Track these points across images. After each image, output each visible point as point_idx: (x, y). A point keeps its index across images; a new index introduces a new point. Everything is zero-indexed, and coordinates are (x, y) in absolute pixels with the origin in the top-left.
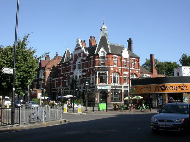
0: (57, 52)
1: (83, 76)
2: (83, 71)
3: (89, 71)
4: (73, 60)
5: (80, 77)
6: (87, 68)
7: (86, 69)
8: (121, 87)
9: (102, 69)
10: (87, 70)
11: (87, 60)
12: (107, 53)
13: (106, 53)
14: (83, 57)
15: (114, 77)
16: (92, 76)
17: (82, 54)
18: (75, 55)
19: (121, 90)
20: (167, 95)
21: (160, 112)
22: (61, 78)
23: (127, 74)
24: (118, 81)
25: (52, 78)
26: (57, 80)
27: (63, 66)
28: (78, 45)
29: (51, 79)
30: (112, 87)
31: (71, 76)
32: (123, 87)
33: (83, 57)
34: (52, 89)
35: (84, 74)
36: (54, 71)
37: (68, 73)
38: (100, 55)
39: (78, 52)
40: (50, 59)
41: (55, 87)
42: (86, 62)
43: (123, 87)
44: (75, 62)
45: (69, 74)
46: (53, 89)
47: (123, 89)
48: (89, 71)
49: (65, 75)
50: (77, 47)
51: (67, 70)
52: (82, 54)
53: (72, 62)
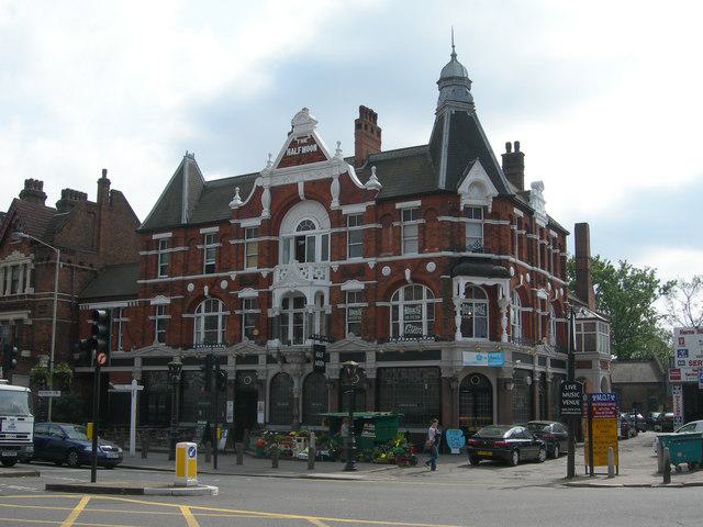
0: (105, 172)
4: (266, 213)
5: (320, 297)
6: (377, 255)
10: (379, 266)
11: (376, 220)
12: (496, 193)
13: (493, 191)
15: (207, 318)
17: (335, 187)
20: (489, 418)
26: (126, 311)
27: (173, 242)
31: (249, 293)
32: (138, 362)
37: (218, 280)
38: (464, 202)
39: (300, 176)
42: (373, 226)
43: (138, 362)
44: (272, 226)
45: (224, 284)
48: (191, 287)
52: (335, 187)
53: (246, 223)
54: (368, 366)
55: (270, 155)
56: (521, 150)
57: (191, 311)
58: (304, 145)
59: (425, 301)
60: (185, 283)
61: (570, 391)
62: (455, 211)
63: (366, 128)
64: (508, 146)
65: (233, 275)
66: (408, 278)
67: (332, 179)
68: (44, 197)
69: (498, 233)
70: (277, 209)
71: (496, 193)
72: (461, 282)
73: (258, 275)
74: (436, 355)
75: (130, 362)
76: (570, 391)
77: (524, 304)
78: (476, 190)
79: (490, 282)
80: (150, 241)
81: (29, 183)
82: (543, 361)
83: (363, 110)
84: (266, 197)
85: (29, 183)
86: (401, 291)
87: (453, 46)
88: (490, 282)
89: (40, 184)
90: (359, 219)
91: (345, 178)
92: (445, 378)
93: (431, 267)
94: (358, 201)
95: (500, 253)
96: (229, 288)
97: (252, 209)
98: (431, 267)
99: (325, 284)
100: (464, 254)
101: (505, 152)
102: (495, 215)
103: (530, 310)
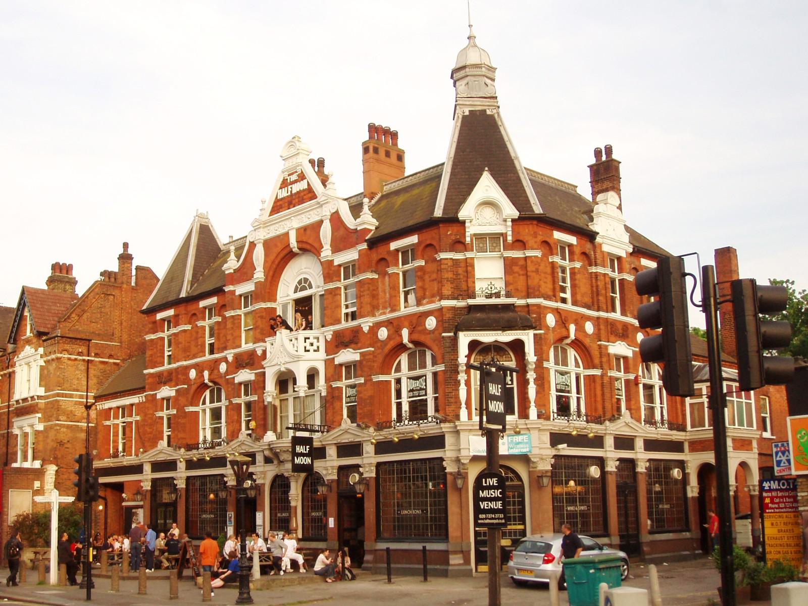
0: (126, 246)
1: (334, 371)
2: (340, 342)
3: (383, 333)
4: (259, 274)
5: (312, 377)
8: (598, 442)
9: (493, 315)
12: (515, 214)
13: (511, 212)
14: (336, 249)
16: (212, 402)
18: (267, 244)
19: (681, 464)
20: (522, 527)
22: (166, 392)
23: (625, 358)
24: (578, 399)
25: (98, 398)
26: (126, 410)
28: (294, 177)
29: (88, 407)
30: (556, 439)
31: (245, 375)
32: (609, 442)
33: (336, 249)
35: (348, 356)
36: (111, 356)
37: (217, 362)
38: (471, 230)
40: (80, 290)
41: (116, 455)
43: (609, 442)
44: (268, 290)
45: (223, 367)
46: (108, 462)
47: (612, 455)
48: (193, 374)
49: (193, 374)
50: (284, 194)
51: (208, 341)
53: (242, 289)
54: (366, 461)
55: (263, 202)
56: (614, 156)
57: (194, 402)
58: (295, 182)
59: (429, 370)
60: (187, 368)
61: (490, 488)
62: (459, 244)
63: (388, 154)
64: (598, 153)
65: (230, 354)
66: (405, 340)
67: (321, 222)
68: (73, 282)
69: (525, 267)
70: (273, 262)
71: (515, 214)
72: (465, 339)
73: (252, 353)
74: (438, 442)
75: (598, 442)
76: (490, 488)
77: (589, 363)
78: (488, 212)
79: (506, 337)
80: (155, 322)
81: (56, 267)
82: (623, 442)
83: (374, 129)
84: (259, 255)
85: (56, 267)
86: (404, 359)
87: (470, 26)
88: (506, 337)
89: (68, 268)
90: (350, 269)
91: (336, 218)
92: (451, 474)
93: (431, 323)
94: (352, 245)
95: (528, 296)
96: (227, 373)
97: (245, 272)
98: (431, 323)
99: (318, 360)
100: (471, 302)
101: (593, 161)
102: (520, 244)
103: (597, 372)
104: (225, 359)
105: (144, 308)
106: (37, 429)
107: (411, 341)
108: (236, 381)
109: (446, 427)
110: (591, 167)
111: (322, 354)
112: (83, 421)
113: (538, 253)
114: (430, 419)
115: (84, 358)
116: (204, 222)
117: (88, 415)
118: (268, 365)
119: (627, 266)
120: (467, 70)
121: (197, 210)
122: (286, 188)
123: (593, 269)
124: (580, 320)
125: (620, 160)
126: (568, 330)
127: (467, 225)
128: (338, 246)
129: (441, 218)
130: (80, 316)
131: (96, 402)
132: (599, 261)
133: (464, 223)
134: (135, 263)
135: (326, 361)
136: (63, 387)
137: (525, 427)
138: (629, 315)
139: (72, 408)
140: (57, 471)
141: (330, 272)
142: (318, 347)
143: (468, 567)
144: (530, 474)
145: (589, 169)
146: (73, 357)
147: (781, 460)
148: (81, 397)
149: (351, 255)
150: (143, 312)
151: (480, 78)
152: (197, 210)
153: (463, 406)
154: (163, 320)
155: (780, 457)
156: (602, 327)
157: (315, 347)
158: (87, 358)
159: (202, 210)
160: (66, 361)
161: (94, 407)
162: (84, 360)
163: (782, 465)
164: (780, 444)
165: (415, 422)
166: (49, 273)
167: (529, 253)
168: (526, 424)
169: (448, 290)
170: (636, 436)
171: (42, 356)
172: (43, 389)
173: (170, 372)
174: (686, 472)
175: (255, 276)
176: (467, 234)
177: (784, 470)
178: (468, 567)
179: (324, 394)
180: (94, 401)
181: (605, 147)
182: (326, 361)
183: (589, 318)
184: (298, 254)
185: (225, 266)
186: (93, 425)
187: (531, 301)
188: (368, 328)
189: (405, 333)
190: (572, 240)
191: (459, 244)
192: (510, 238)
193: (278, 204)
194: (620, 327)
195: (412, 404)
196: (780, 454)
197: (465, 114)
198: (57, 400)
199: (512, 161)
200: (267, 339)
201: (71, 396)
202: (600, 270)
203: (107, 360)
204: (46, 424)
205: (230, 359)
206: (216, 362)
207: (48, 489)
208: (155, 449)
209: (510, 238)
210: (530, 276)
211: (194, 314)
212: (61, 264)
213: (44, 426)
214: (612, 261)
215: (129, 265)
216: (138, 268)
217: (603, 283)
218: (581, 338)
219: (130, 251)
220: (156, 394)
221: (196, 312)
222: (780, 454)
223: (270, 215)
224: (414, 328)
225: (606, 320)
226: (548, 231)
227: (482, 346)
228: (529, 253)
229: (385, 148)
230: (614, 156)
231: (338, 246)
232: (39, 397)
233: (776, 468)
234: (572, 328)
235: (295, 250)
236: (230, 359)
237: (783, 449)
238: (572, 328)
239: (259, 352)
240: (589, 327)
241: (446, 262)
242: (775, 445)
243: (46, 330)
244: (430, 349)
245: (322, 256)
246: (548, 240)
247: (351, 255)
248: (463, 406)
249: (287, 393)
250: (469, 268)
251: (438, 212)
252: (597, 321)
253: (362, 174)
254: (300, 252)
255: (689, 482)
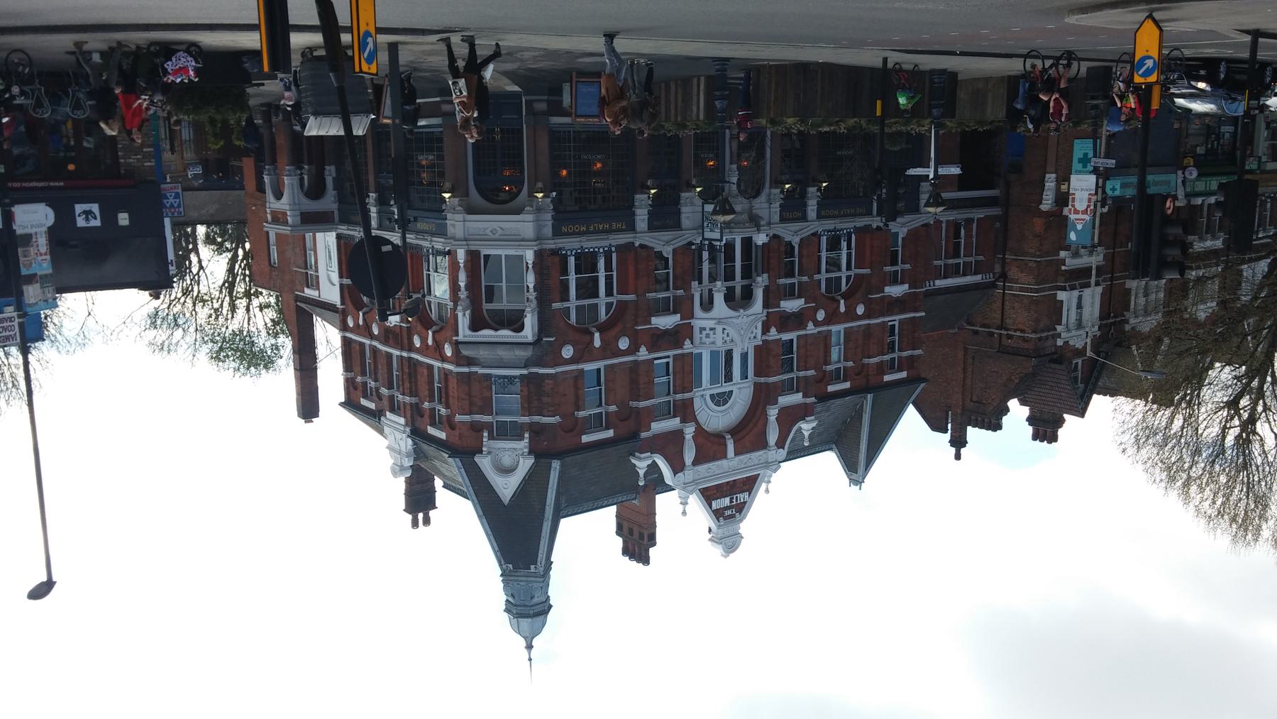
0: (958, 457)
1: (682, 307)
4: (773, 413)
7: (780, 331)
10: (633, 349)
12: (477, 459)
13: (484, 462)
14: (678, 436)
18: (763, 445)
21: (464, 134)
25: (993, 285)
31: (792, 305)
33: (678, 436)
34: (995, 211)
36: (976, 332)
38: (523, 445)
39: (730, 466)
42: (643, 404)
44: (763, 396)
45: (821, 315)
46: (979, 214)
48: (860, 310)
49: (860, 310)
50: (742, 497)
53: (796, 398)
58: (727, 508)
60: (866, 316)
62: (537, 431)
64: (427, 521)
65: (811, 328)
66: (597, 335)
67: (695, 463)
69: (471, 404)
71: (477, 459)
78: (507, 460)
81: (1053, 438)
83: (643, 558)
85: (1053, 438)
86: (603, 316)
87: (530, 659)
88: (486, 334)
91: (678, 467)
96: (816, 310)
97: (790, 418)
99: (701, 320)
101: (432, 513)
102: (477, 428)
104: (817, 324)
105: (923, 385)
106: (1067, 252)
107: (592, 334)
108: (803, 300)
109: (551, 245)
110: (434, 507)
111: (697, 324)
112: (1009, 260)
113: (458, 418)
114: (601, 250)
115: (1006, 333)
116: (854, 476)
117: (1003, 267)
118: (760, 316)
119: (386, 402)
120: (531, 612)
121: (860, 489)
122: (739, 502)
123: (414, 400)
124: (424, 350)
125: (404, 512)
126: (434, 339)
127: (526, 450)
128: (675, 438)
129: (554, 459)
130: (1010, 380)
131: (995, 281)
132: (408, 407)
133: (530, 453)
134: (947, 436)
135: (692, 317)
136: (1030, 299)
137: (469, 242)
138: (384, 353)
139: (1020, 275)
140: (1041, 203)
141: (685, 411)
142: (701, 333)
143: (529, 98)
144: (467, 195)
145: (437, 506)
146: (1018, 334)
147: (171, 203)
148: (1011, 288)
149: (658, 427)
150: (924, 380)
151: (518, 603)
152: (860, 489)
153: (530, 266)
154: (900, 370)
155: (175, 202)
156: (406, 341)
157: (704, 332)
158: (1003, 332)
159: (855, 488)
160: (1026, 329)
161: (997, 275)
162: (1007, 329)
163: (173, 194)
164: (176, 214)
165: (587, 250)
166: (1061, 432)
167: (466, 418)
168: (467, 245)
169: (548, 384)
170: (377, 230)
171: (1059, 336)
172: (1059, 298)
173: (890, 312)
174: (336, 192)
175: (777, 411)
176: (527, 441)
177: (171, 188)
178: (529, 98)
179: (695, 284)
180: (997, 283)
181: (418, 527)
182: (692, 317)
183: (418, 351)
184: (727, 432)
185: (814, 424)
186: (999, 256)
187: (465, 370)
188: (641, 350)
189: (597, 342)
190: (432, 431)
191: (537, 431)
192: (485, 434)
193: (747, 487)
194: (391, 341)
195: (594, 268)
196: (176, 205)
197: (534, 566)
198: (1038, 285)
199: (484, 514)
200: (761, 343)
201: (1021, 289)
202: (407, 399)
203: (980, 329)
204: (1058, 257)
205: (810, 325)
206: (830, 321)
207: (1051, 182)
208: (910, 228)
209: (485, 434)
210: (466, 395)
211: (858, 374)
212: (1038, 440)
213: (1059, 255)
214: (399, 408)
215: (954, 434)
216: (945, 431)
217: (405, 386)
218: (424, 331)
219: (953, 450)
220: (909, 289)
221: (856, 377)
222: (176, 205)
223: (759, 474)
224: (587, 347)
225: (402, 349)
226: (450, 440)
227: (512, 327)
228: (466, 418)
229: (634, 538)
230: (409, 517)
231: (675, 438)
232: (1064, 289)
233: (180, 191)
234: (430, 342)
235: (728, 436)
236: (810, 325)
237: (173, 210)
238: (430, 342)
239: (773, 330)
240: (417, 342)
241: (550, 413)
242: (181, 213)
243: (1053, 366)
244: (571, 326)
245: (694, 428)
246: (450, 430)
247: (658, 427)
248: (530, 266)
249: (742, 286)
250: (526, 405)
251: (556, 465)
252: (411, 348)
253: (657, 512)
254: (724, 434)
255: (333, 181)
